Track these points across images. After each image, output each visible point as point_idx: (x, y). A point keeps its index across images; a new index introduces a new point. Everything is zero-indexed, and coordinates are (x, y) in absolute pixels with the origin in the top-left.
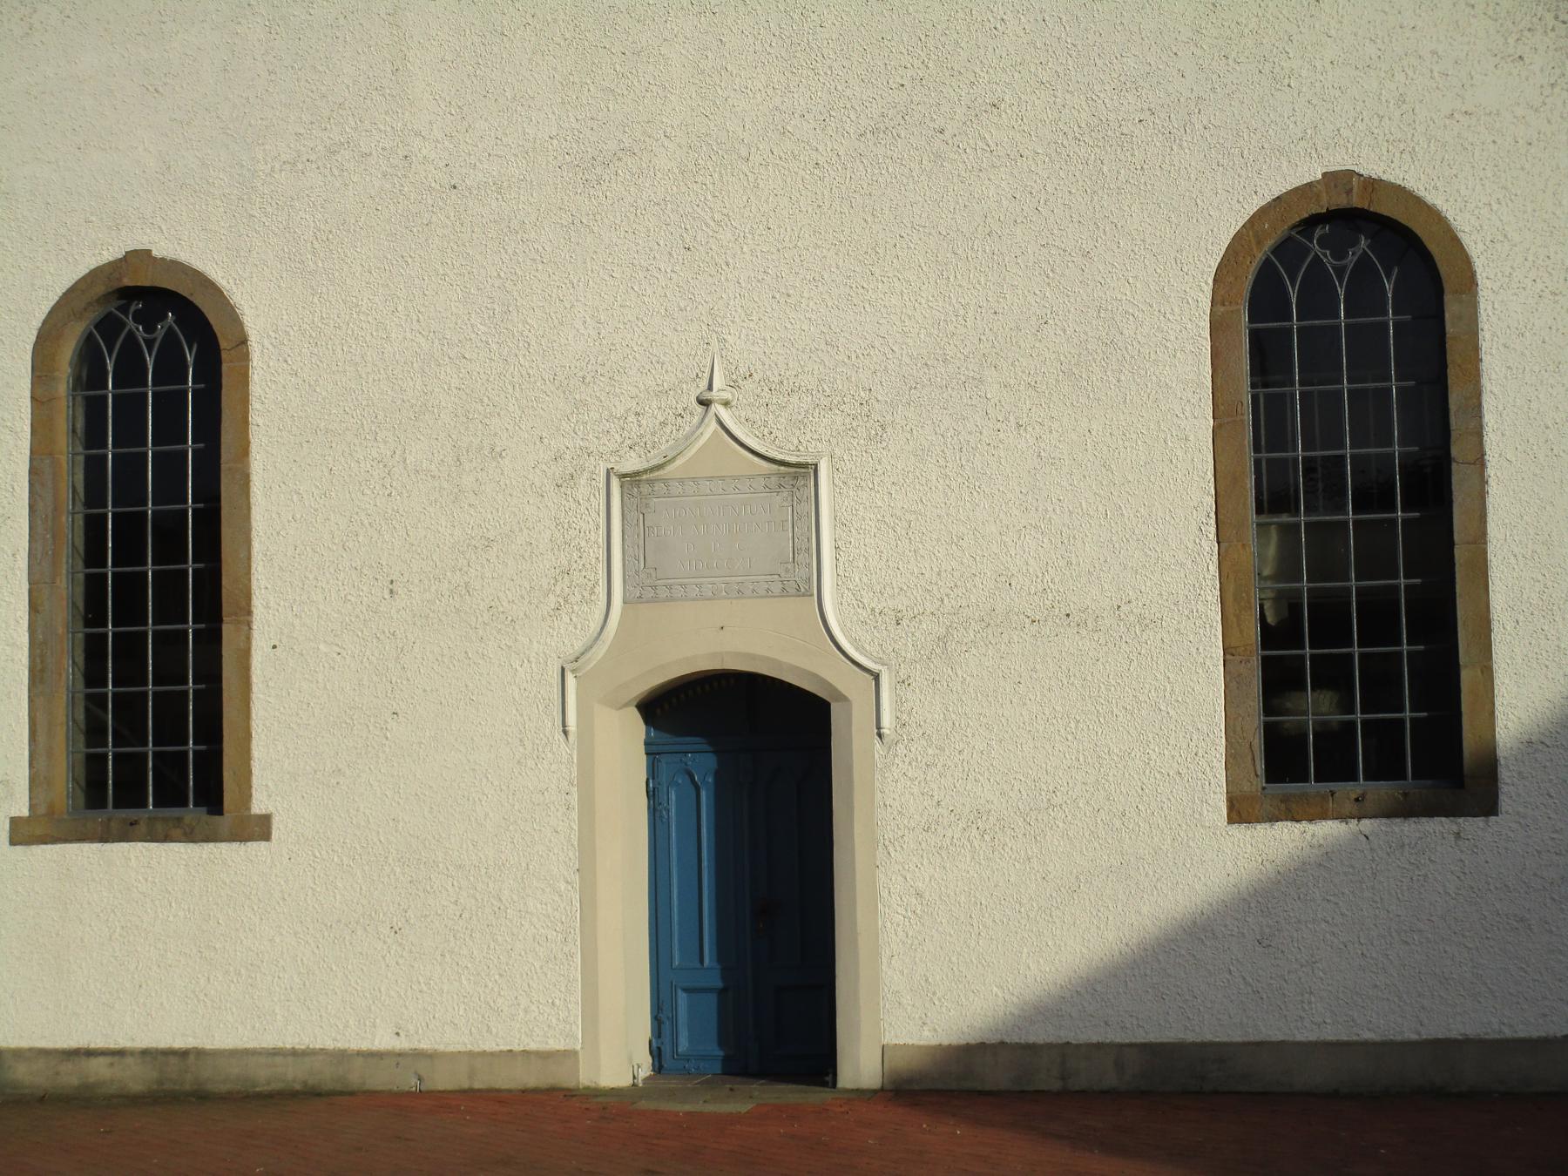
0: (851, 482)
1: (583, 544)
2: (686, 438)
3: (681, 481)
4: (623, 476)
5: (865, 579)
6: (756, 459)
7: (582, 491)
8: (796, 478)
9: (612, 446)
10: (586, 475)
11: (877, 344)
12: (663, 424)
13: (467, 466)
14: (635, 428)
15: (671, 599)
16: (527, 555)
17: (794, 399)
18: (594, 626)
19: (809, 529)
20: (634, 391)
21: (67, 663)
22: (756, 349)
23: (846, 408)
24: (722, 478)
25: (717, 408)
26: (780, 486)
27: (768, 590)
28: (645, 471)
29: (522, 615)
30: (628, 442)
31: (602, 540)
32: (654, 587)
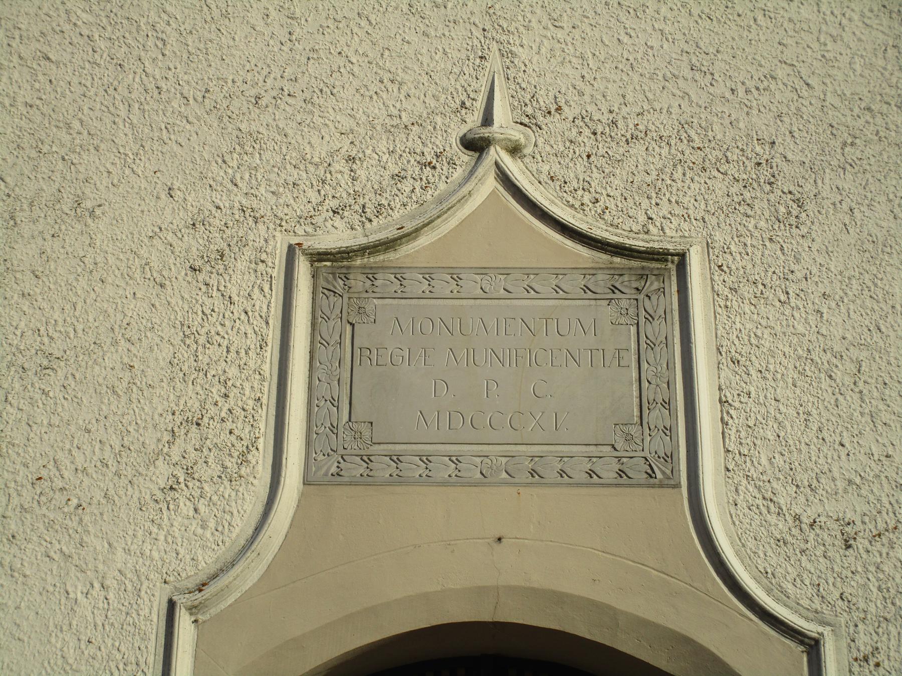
0: (747, 290)
1: (233, 372)
2: (440, 201)
3: (429, 274)
4: (318, 257)
5: (779, 461)
6: (569, 243)
7: (239, 277)
8: (643, 277)
9: (301, 208)
10: (248, 253)
11: (780, 73)
12: (398, 177)
13: (26, 229)
14: (344, 180)
15: (399, 480)
16: (121, 388)
17: (638, 149)
18: (242, 526)
19: (669, 366)
20: (347, 123)
21: (260, 506)
22: (568, 70)
23: (732, 170)
24: (506, 272)
25: (496, 153)
26: (614, 289)
27: (591, 473)
28: (363, 250)
29: (98, 495)
30: (334, 204)
31: (270, 367)
32: (367, 459)
